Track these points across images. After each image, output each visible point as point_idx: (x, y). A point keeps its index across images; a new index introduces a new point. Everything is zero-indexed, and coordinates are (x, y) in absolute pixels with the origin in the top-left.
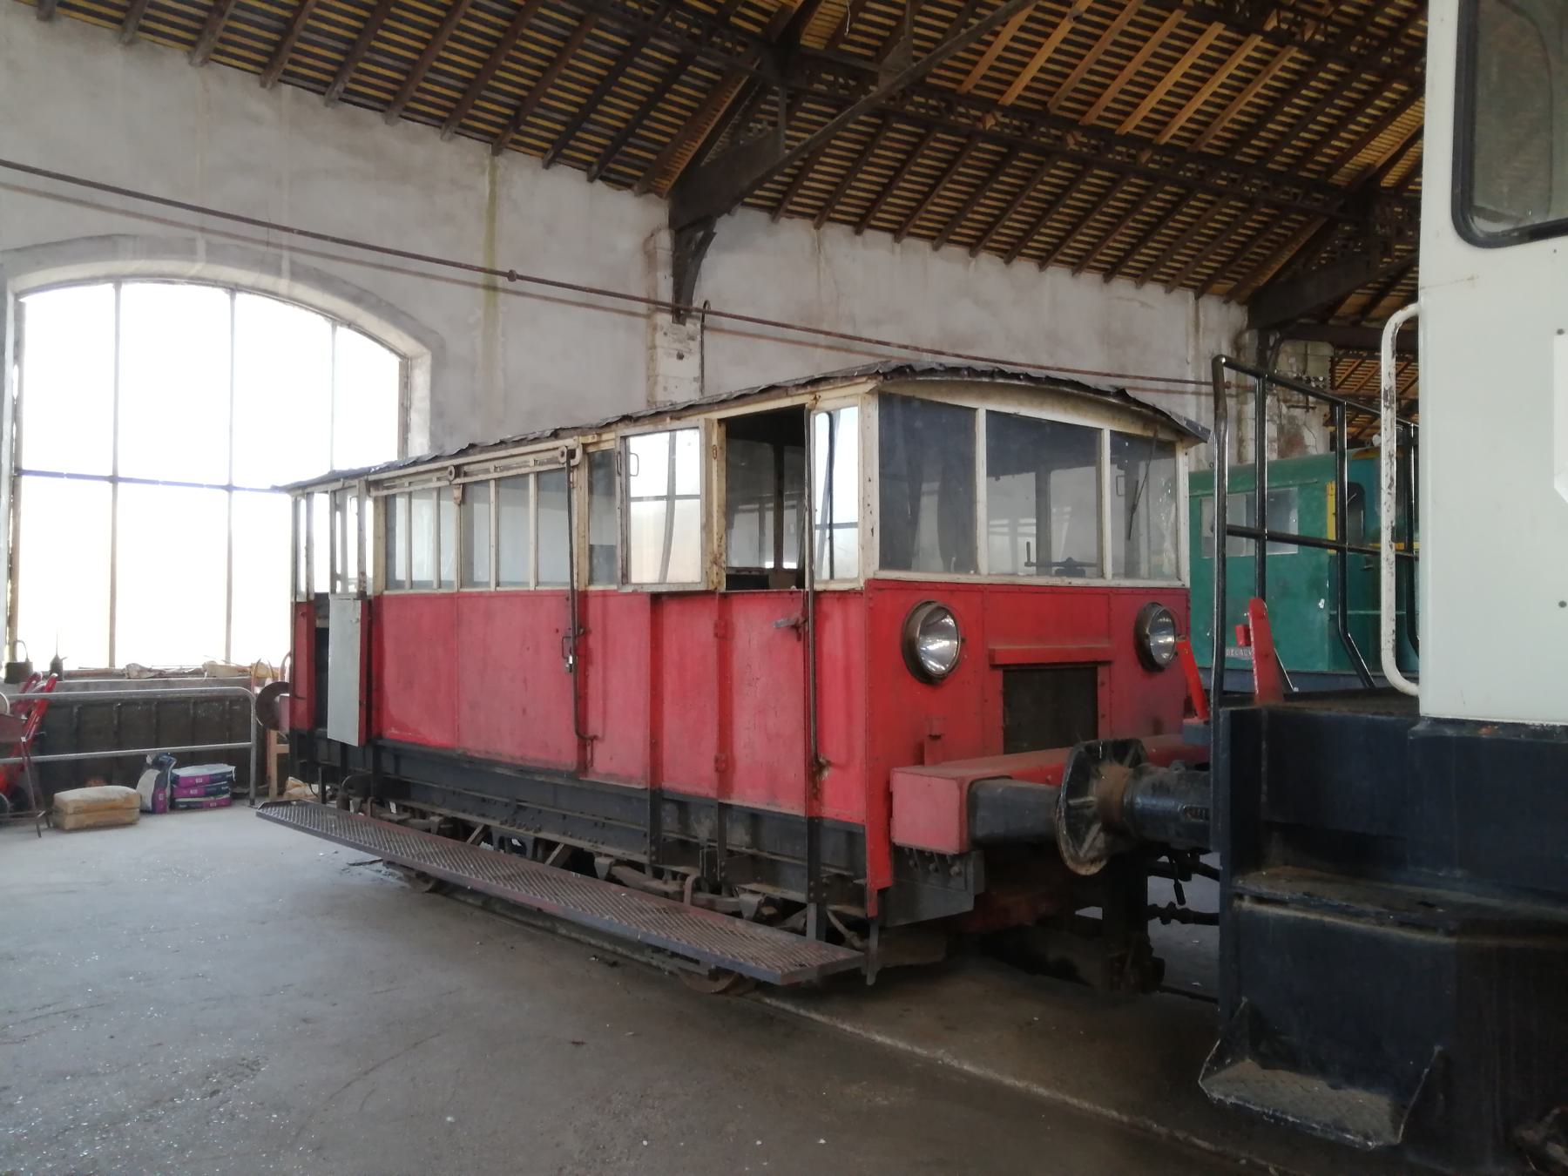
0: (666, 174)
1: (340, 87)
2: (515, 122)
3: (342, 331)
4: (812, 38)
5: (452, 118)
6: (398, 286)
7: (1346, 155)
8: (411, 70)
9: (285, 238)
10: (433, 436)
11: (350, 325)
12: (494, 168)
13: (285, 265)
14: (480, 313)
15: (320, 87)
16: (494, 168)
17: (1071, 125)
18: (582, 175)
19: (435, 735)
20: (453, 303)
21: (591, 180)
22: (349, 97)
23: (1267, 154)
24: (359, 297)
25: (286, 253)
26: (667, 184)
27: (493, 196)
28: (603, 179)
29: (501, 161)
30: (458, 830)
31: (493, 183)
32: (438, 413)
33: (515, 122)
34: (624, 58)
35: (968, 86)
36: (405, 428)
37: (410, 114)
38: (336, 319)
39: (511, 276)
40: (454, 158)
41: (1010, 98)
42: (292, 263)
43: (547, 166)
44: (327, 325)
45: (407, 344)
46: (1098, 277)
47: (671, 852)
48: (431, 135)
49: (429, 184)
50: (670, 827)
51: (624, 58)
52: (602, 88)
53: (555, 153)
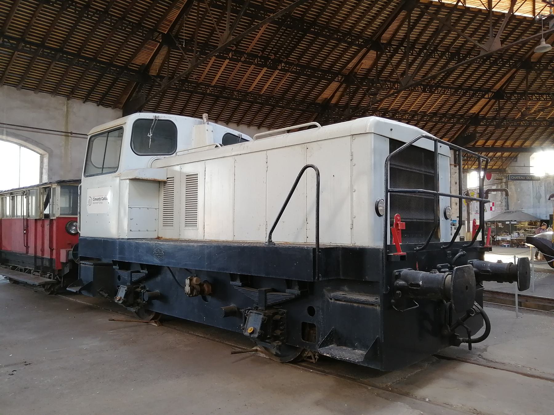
0: (121, 103)
1: (20, 86)
2: (72, 92)
3: (22, 148)
4: (153, 72)
5: (55, 91)
6: (38, 136)
7: (318, 96)
8: (40, 81)
9: (5, 126)
10: (49, 176)
11: (25, 147)
12: (68, 104)
13: (5, 132)
14: (64, 143)
15: (15, 86)
16: (68, 104)
17: (234, 90)
18: (95, 104)
19: (9, 249)
20: (57, 140)
21: (98, 105)
22: (23, 88)
23: (295, 96)
24: (27, 140)
25: (5, 129)
26: (122, 106)
27: (67, 110)
28: (102, 105)
29: (69, 101)
30: (14, 268)
31: (67, 108)
32: (50, 170)
33: (72, 92)
34: (100, 77)
35: (200, 81)
36: (41, 173)
37: (42, 91)
38: (21, 145)
39: (71, 133)
40: (56, 103)
41: (214, 83)
42: (7, 132)
43: (84, 102)
44: (19, 147)
45: (42, 151)
46: (256, 128)
47: (37, 269)
48: (49, 96)
49: (49, 109)
50: (39, 263)
51: (100, 77)
52: (96, 83)
53: (86, 99)
